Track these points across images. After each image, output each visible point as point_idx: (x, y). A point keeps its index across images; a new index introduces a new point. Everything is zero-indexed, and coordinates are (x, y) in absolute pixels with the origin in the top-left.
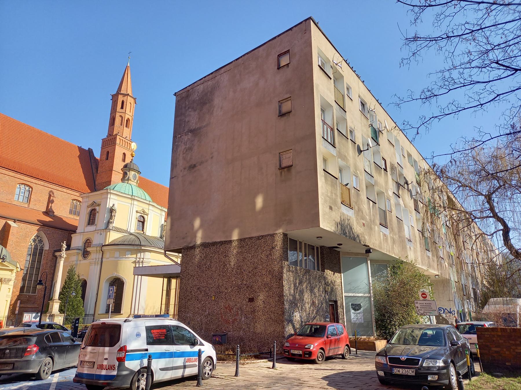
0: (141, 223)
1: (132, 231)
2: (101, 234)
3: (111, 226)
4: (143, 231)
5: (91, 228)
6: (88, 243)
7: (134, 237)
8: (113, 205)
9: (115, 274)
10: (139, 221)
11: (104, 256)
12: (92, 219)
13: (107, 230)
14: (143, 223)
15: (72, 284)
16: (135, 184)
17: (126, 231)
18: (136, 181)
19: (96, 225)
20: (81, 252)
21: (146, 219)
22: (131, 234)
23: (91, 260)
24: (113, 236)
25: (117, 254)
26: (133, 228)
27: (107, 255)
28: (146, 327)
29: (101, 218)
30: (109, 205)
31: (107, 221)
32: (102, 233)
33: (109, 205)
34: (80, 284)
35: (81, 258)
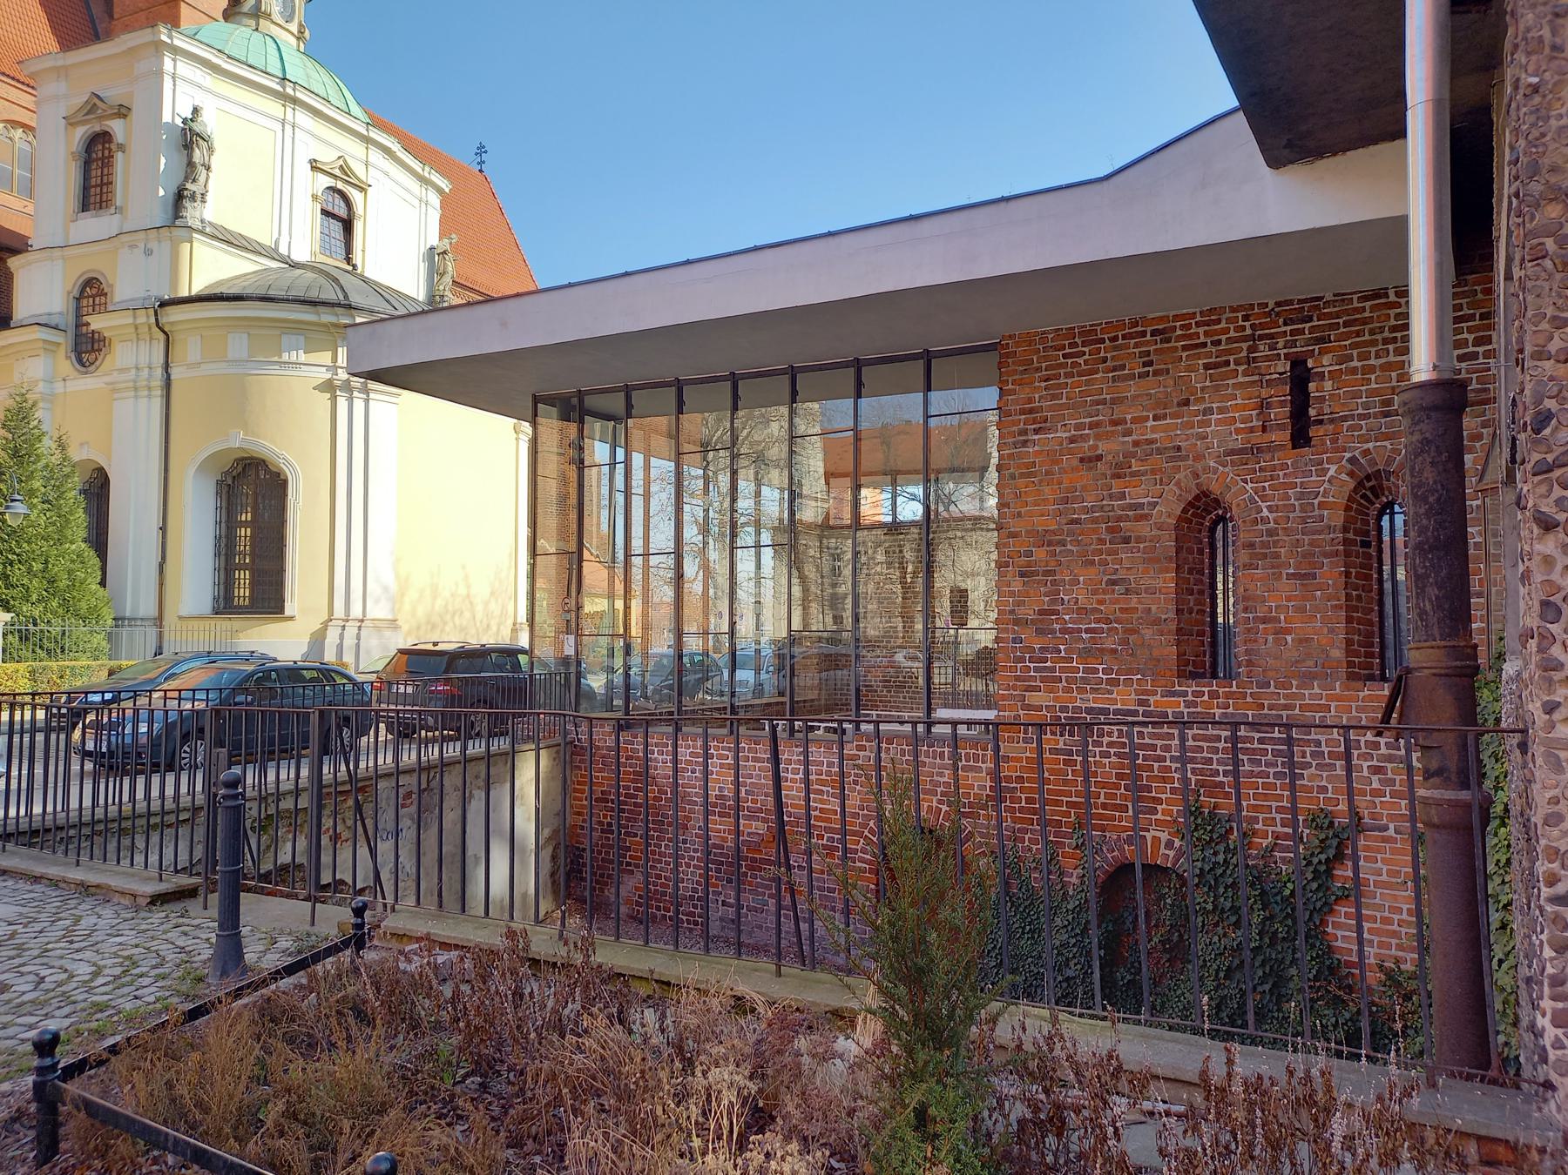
0: (337, 227)
1: (301, 254)
2: (148, 252)
3: (192, 214)
4: (348, 260)
5: (96, 225)
6: (91, 292)
7: (310, 275)
8: (196, 110)
9: (238, 440)
10: (325, 212)
11: (176, 352)
12: (94, 192)
13: (177, 232)
14: (348, 225)
15: (31, 477)
16: (293, 41)
17: (272, 253)
18: (294, 27)
19: (119, 210)
20: (64, 341)
21: (359, 209)
22: (295, 265)
23: (116, 376)
24: (208, 267)
25: (238, 345)
26: (304, 240)
27: (189, 349)
28: (68, 41)
29: (142, 177)
30: (175, 105)
31: (173, 189)
32: (153, 245)
33: (175, 105)
34: (77, 481)
35: (66, 366)
